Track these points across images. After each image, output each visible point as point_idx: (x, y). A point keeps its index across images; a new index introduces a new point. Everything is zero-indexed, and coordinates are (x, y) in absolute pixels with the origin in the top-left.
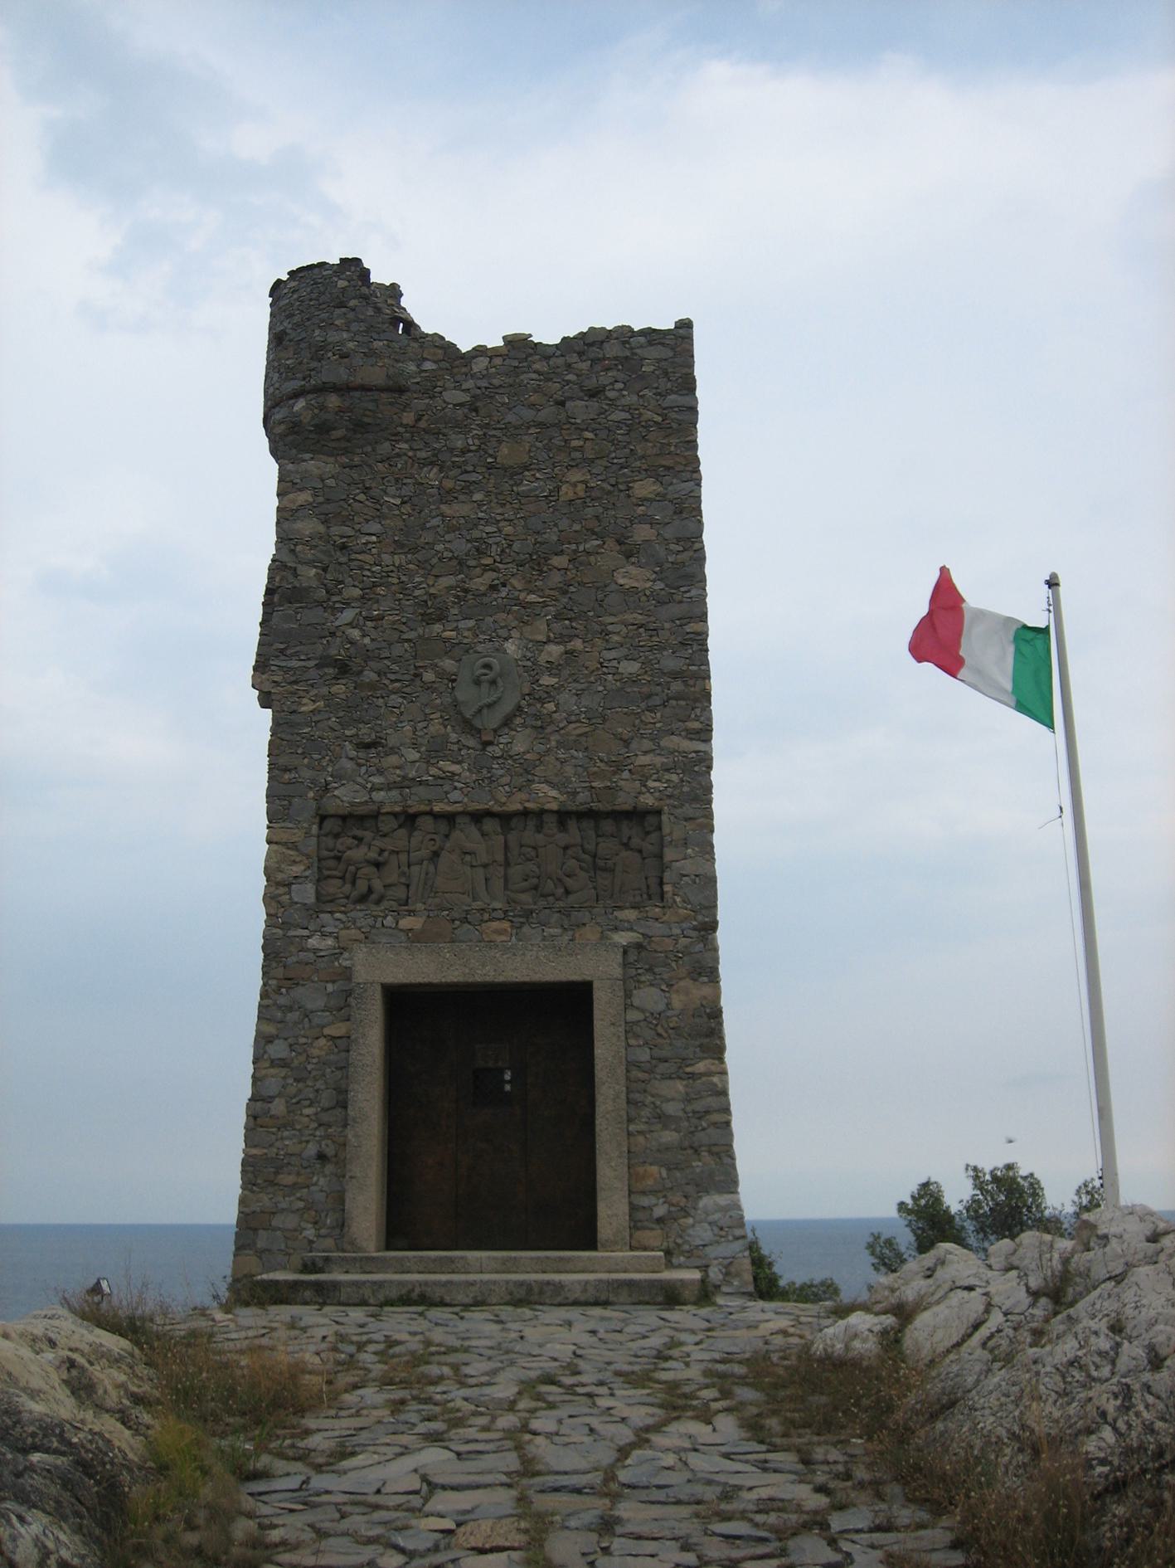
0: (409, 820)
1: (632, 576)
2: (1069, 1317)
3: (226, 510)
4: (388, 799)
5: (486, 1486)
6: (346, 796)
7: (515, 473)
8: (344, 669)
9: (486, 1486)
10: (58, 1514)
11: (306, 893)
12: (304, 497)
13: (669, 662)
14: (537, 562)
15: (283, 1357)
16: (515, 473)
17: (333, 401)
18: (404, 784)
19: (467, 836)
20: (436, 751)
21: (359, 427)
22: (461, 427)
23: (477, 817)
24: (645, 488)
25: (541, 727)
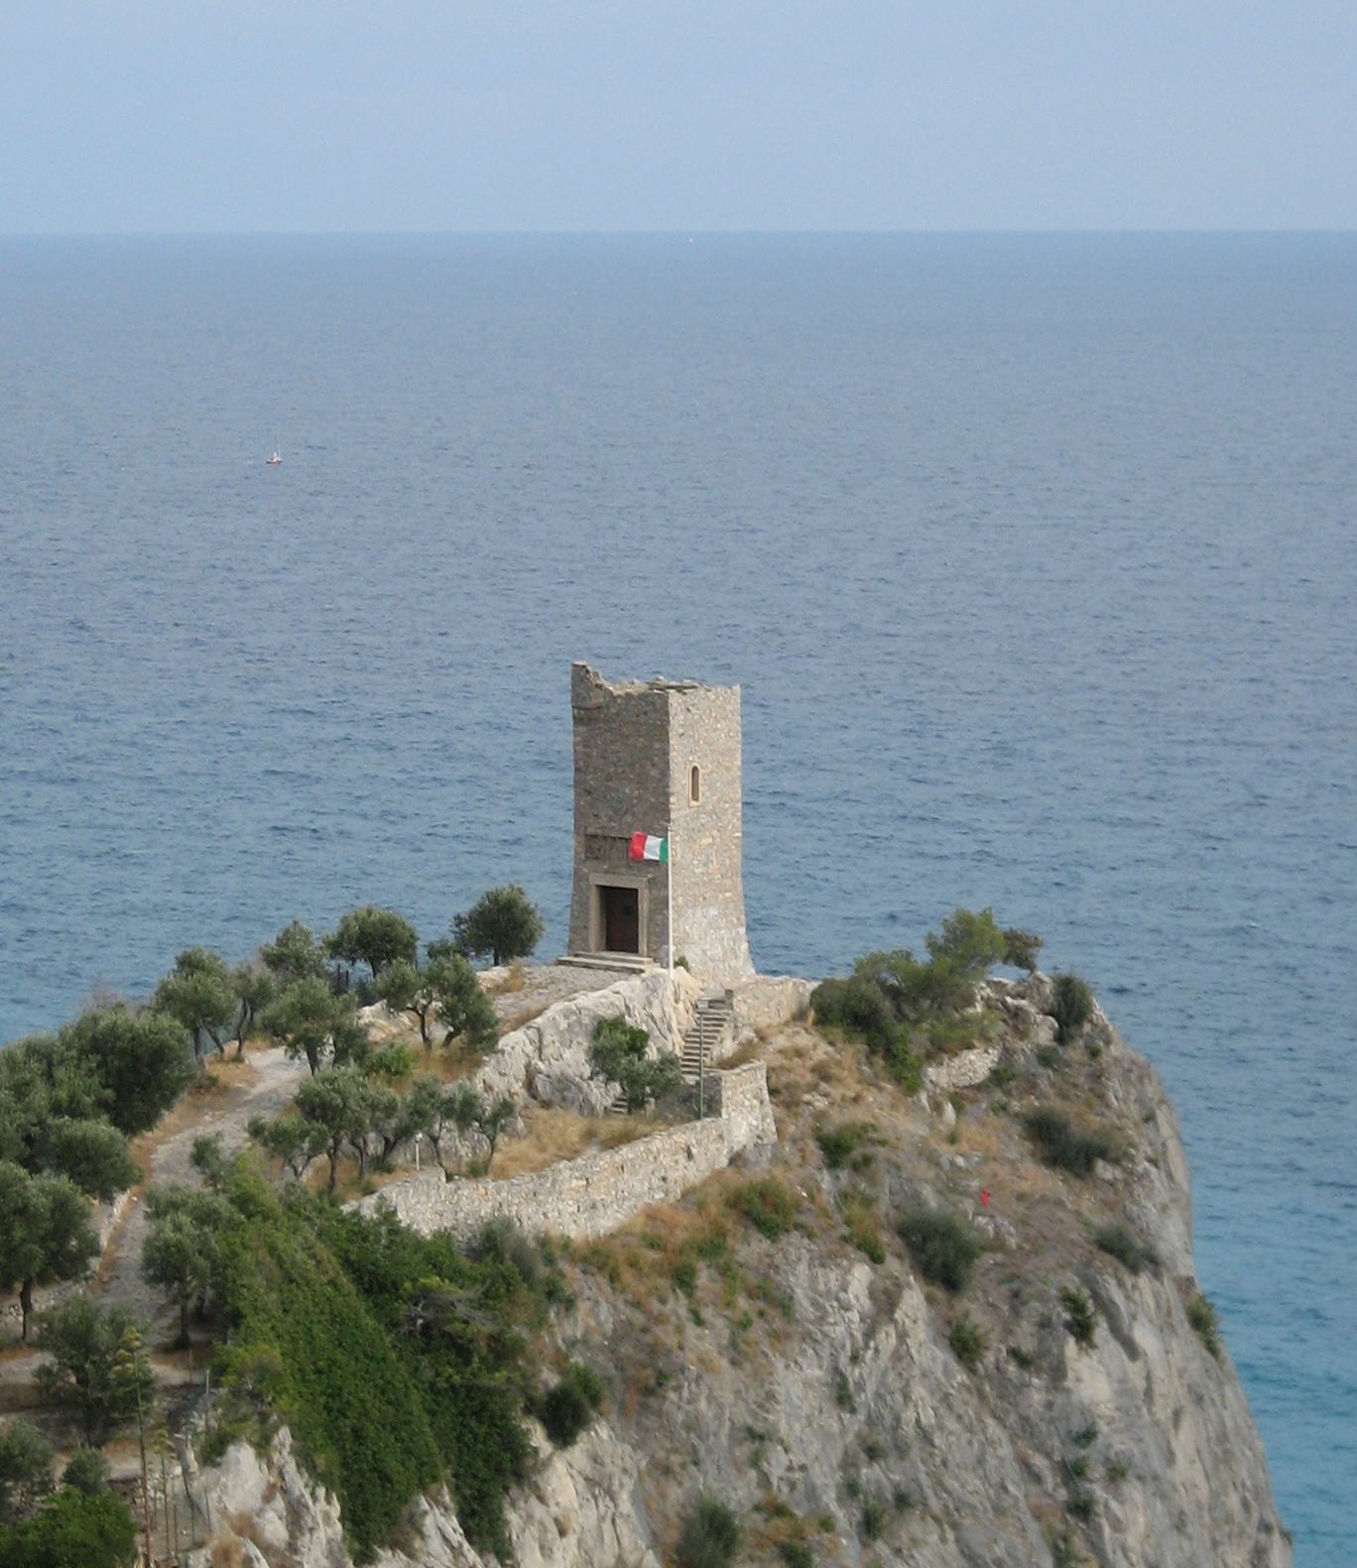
0: (605, 838)
1: (654, 773)
2: (1194, 1461)
3: (563, 739)
4: (599, 832)
5: (599, 967)
6: (591, 830)
7: (627, 737)
8: (589, 793)
9: (599, 967)
10: (549, 1248)
11: (583, 856)
12: (578, 739)
13: (661, 799)
14: (632, 765)
15: (722, 1497)
16: (627, 737)
17: (582, 712)
18: (602, 828)
19: (619, 844)
20: (611, 819)
21: (590, 719)
22: (614, 721)
23: (621, 838)
24: (657, 746)
25: (633, 815)
